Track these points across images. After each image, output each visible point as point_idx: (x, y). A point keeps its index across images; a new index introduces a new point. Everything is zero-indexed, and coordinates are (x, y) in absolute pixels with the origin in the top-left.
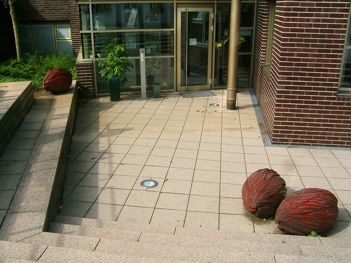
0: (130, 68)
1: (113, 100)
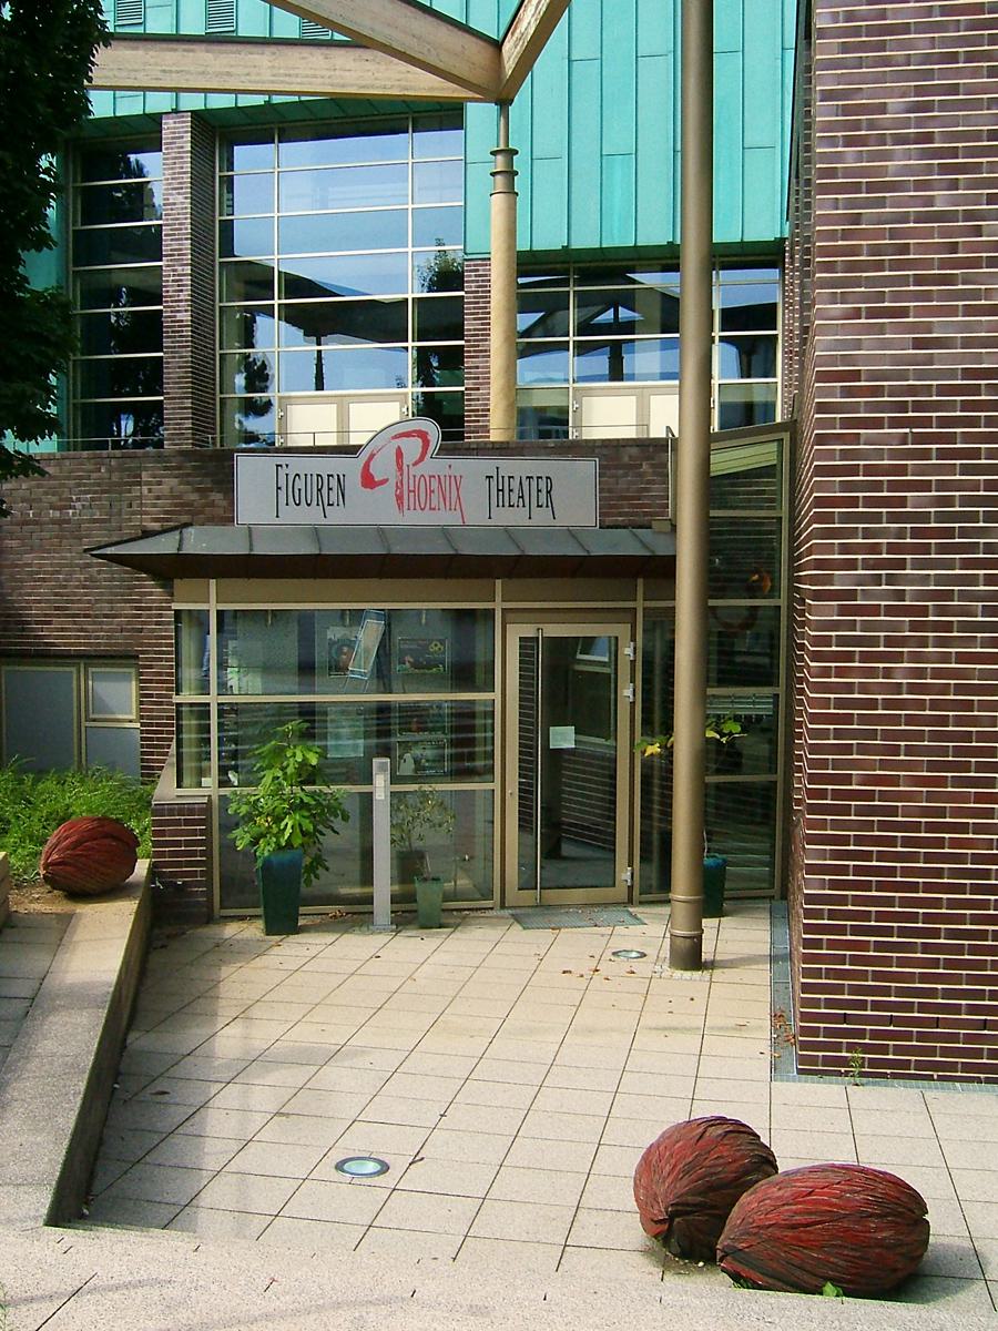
0: (337, 823)
1: (271, 930)
